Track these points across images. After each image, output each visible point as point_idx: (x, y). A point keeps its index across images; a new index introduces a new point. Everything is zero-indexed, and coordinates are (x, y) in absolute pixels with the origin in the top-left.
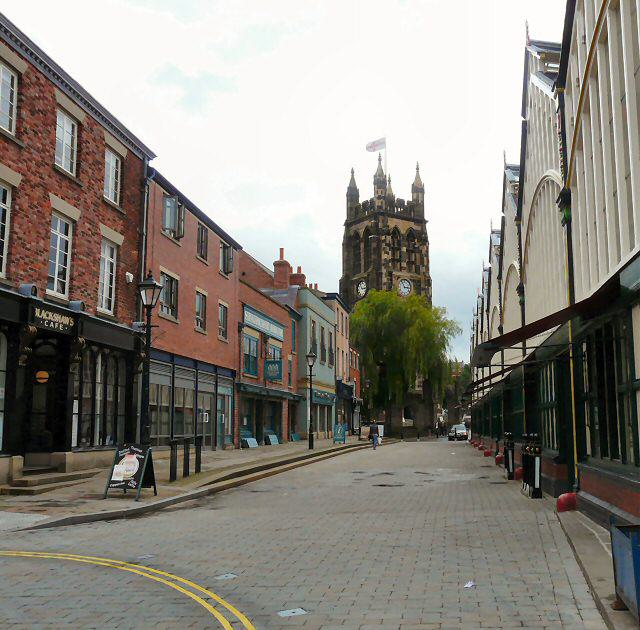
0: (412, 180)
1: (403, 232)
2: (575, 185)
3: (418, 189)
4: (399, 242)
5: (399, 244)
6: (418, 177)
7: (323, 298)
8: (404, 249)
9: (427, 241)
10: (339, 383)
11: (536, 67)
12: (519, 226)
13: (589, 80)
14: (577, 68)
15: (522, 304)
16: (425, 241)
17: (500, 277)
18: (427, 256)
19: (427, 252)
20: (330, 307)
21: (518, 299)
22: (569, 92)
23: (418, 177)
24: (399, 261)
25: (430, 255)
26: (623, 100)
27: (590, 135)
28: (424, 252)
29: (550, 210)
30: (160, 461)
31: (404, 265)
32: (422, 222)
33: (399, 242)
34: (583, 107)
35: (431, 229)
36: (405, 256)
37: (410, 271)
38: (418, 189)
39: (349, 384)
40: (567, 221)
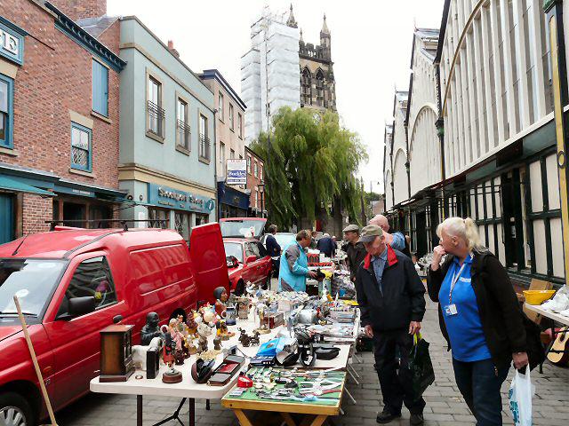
0: (320, 28)
1: (313, 71)
2: (446, 115)
3: (325, 36)
4: (309, 80)
5: (310, 82)
6: (325, 25)
7: (200, 77)
8: (314, 86)
9: (333, 79)
10: (220, 185)
11: (420, 46)
12: (406, 129)
13: (451, 82)
14: (448, 54)
15: (408, 173)
16: (331, 79)
17: (391, 154)
18: (334, 92)
19: (334, 88)
20: (209, 87)
21: (406, 170)
22: (443, 65)
23: (325, 25)
24: (310, 96)
25: (336, 92)
26: (474, 81)
27: (456, 89)
28: (331, 88)
29: (428, 127)
30: (436, 354)
31: (314, 100)
32: (328, 63)
33: (309, 80)
34: (452, 77)
35: (337, 70)
36: (314, 92)
37: (320, 105)
38: (325, 36)
39: (245, 191)
40: (441, 136)
